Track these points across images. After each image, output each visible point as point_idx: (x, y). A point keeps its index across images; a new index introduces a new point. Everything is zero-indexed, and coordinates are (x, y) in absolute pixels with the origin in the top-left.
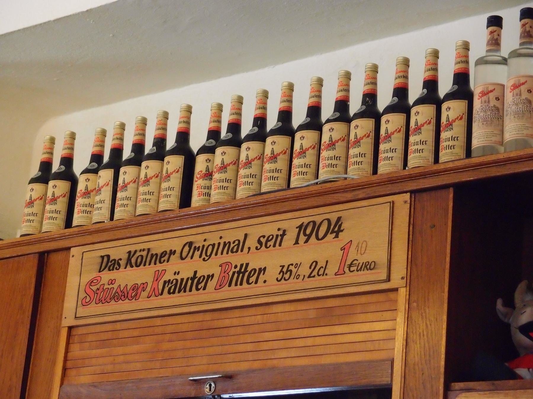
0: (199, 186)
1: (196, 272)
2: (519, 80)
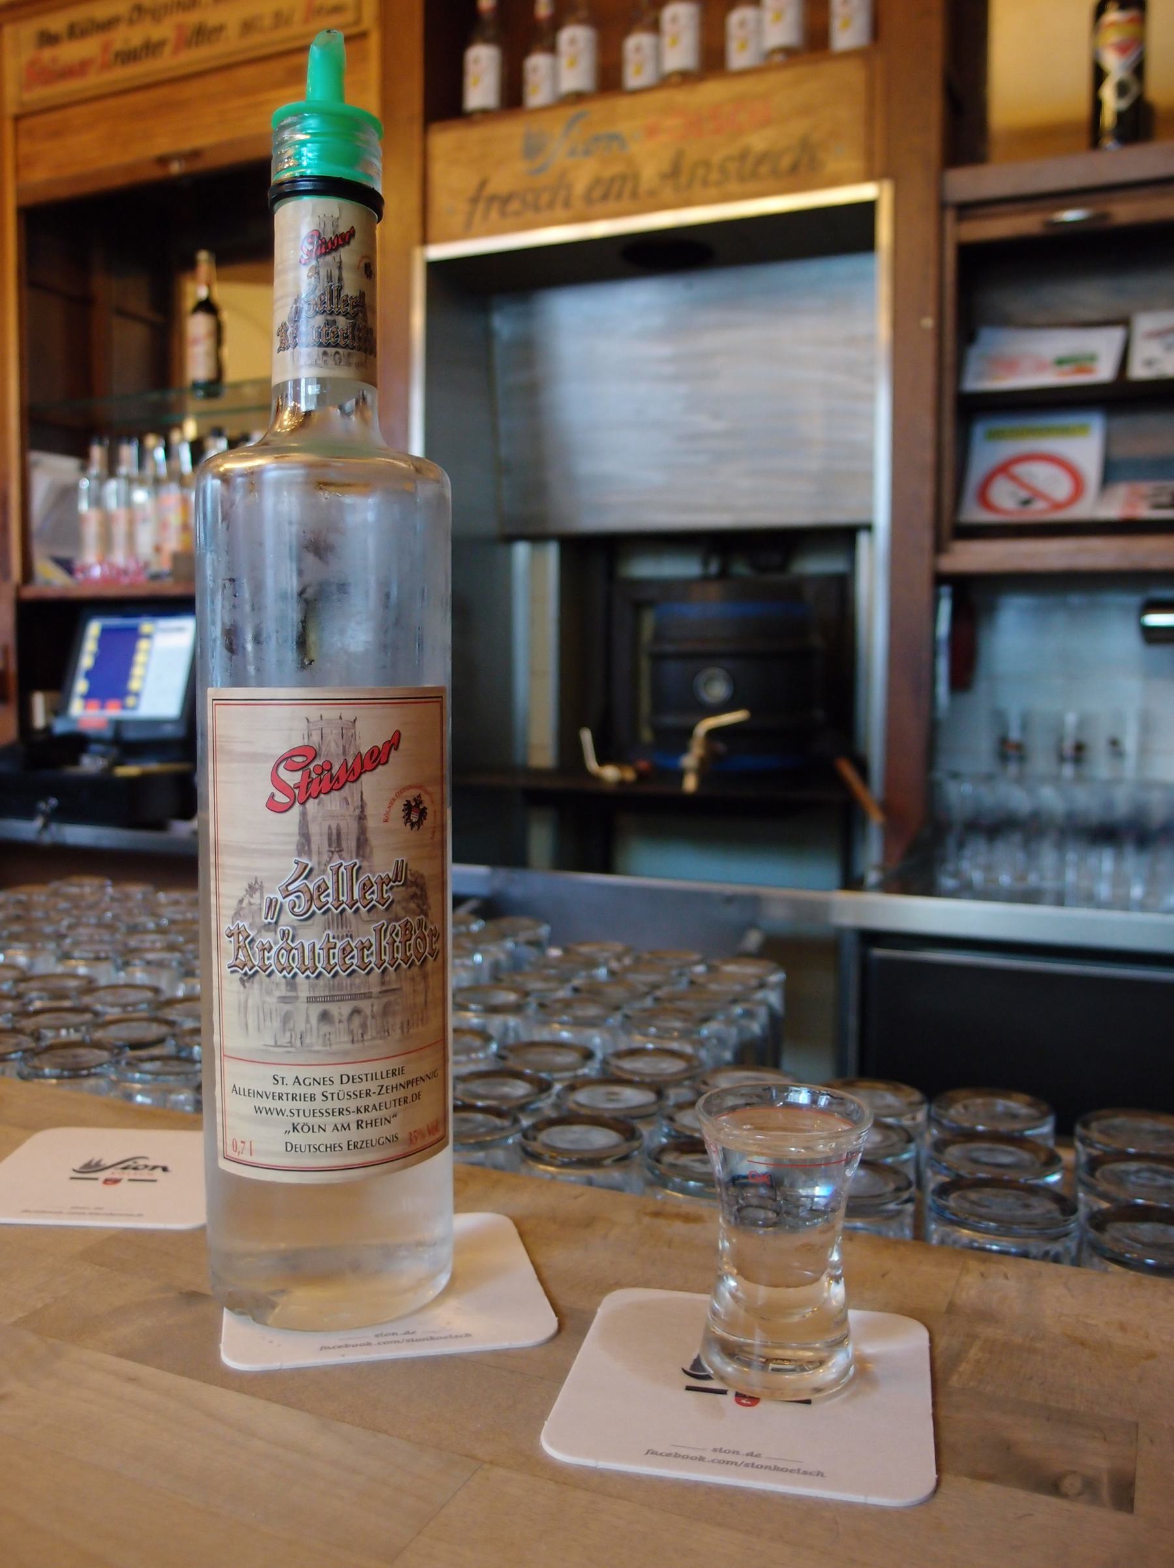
2: (347, 730)
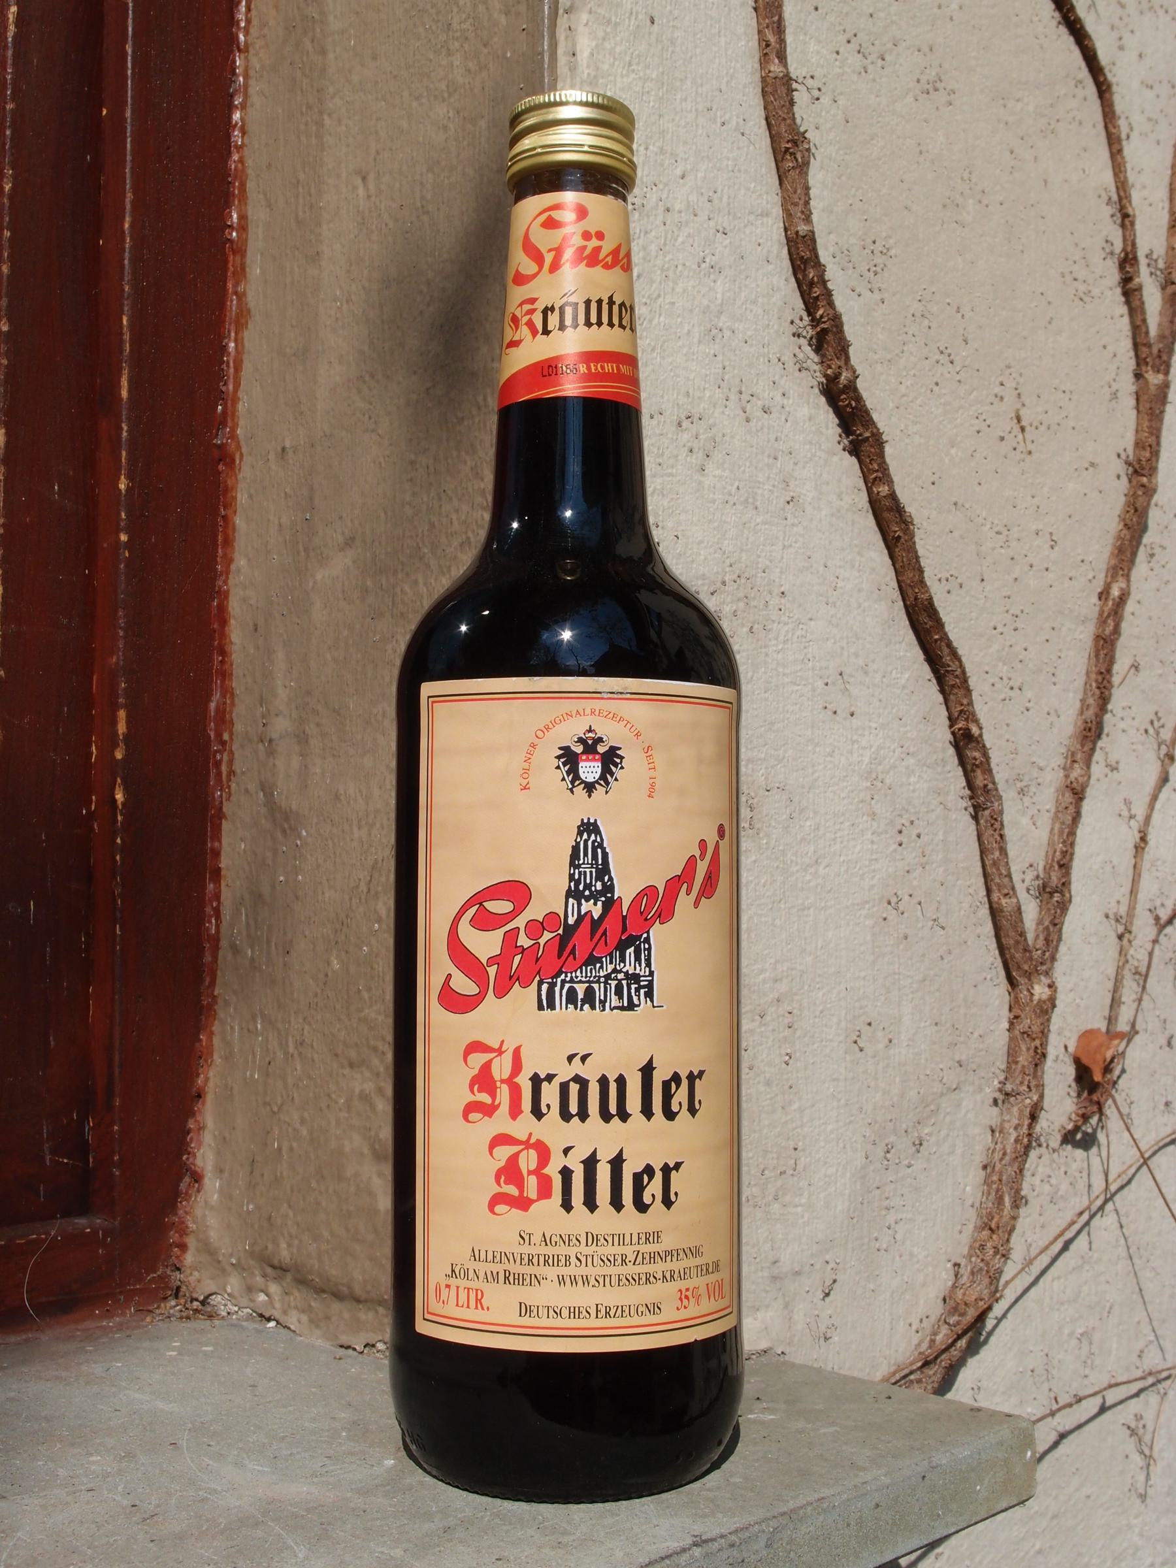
0: (501, 1068)
1: (530, 1135)
